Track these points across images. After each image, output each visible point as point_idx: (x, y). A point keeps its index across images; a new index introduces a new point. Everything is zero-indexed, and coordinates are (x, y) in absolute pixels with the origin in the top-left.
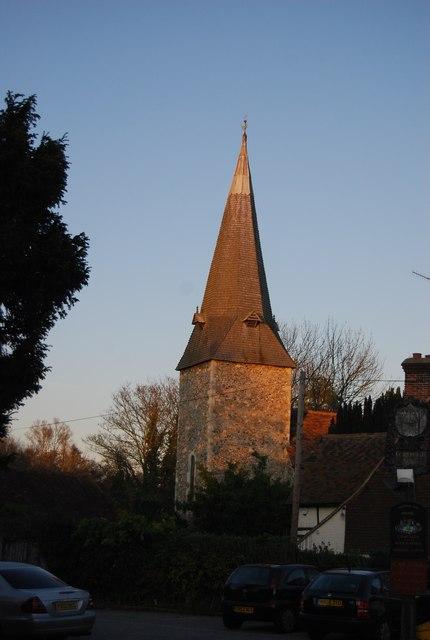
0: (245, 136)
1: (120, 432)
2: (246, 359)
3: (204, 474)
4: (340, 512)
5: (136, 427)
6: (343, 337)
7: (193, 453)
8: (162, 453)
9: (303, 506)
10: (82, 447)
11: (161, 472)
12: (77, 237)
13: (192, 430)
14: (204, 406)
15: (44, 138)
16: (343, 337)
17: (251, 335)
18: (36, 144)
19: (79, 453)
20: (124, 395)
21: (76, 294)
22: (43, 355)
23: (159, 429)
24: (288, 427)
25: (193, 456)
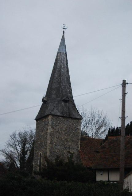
0: (64, 32)
1: (12, 149)
2: (63, 114)
3: (46, 159)
7: (41, 152)
8: (27, 157)
11: (26, 163)
13: (41, 143)
17: (65, 105)
20: (14, 135)
25: (41, 154)
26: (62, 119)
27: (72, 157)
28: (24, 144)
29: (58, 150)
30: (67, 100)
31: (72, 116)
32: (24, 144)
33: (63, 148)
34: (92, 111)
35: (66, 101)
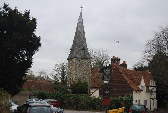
0: (81, 10)
1: (56, 73)
3: (73, 81)
5: (60, 71)
6: (103, 52)
8: (65, 77)
10: (49, 76)
11: (64, 81)
12: (39, 37)
15: (32, 18)
16: (103, 52)
18: (31, 19)
20: (57, 65)
21: (39, 48)
22: (32, 60)
23: (65, 72)
26: (81, 59)
27: (85, 80)
28: (63, 70)
31: (86, 58)
32: (63, 70)
34: (100, 51)
35: (83, 50)
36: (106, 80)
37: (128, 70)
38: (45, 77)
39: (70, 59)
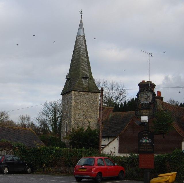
0: (81, 17)
1: (45, 117)
4: (117, 138)
7: (67, 122)
8: (58, 124)
9: (103, 137)
10: (34, 123)
14: (71, 106)
19: (34, 124)
20: (46, 105)
24: (98, 112)
25: (67, 123)
28: (55, 113)
29: (81, 120)
30: (86, 77)
32: (55, 113)
33: (84, 117)
36: (144, 114)
37: (164, 102)
38: (29, 124)
39: (65, 93)
